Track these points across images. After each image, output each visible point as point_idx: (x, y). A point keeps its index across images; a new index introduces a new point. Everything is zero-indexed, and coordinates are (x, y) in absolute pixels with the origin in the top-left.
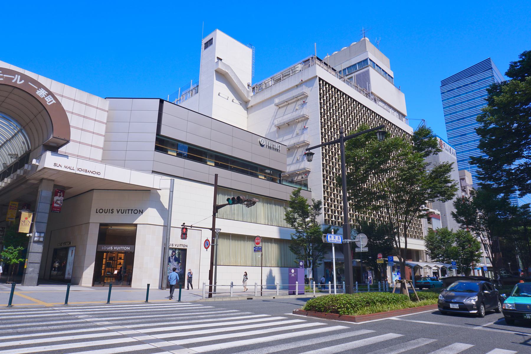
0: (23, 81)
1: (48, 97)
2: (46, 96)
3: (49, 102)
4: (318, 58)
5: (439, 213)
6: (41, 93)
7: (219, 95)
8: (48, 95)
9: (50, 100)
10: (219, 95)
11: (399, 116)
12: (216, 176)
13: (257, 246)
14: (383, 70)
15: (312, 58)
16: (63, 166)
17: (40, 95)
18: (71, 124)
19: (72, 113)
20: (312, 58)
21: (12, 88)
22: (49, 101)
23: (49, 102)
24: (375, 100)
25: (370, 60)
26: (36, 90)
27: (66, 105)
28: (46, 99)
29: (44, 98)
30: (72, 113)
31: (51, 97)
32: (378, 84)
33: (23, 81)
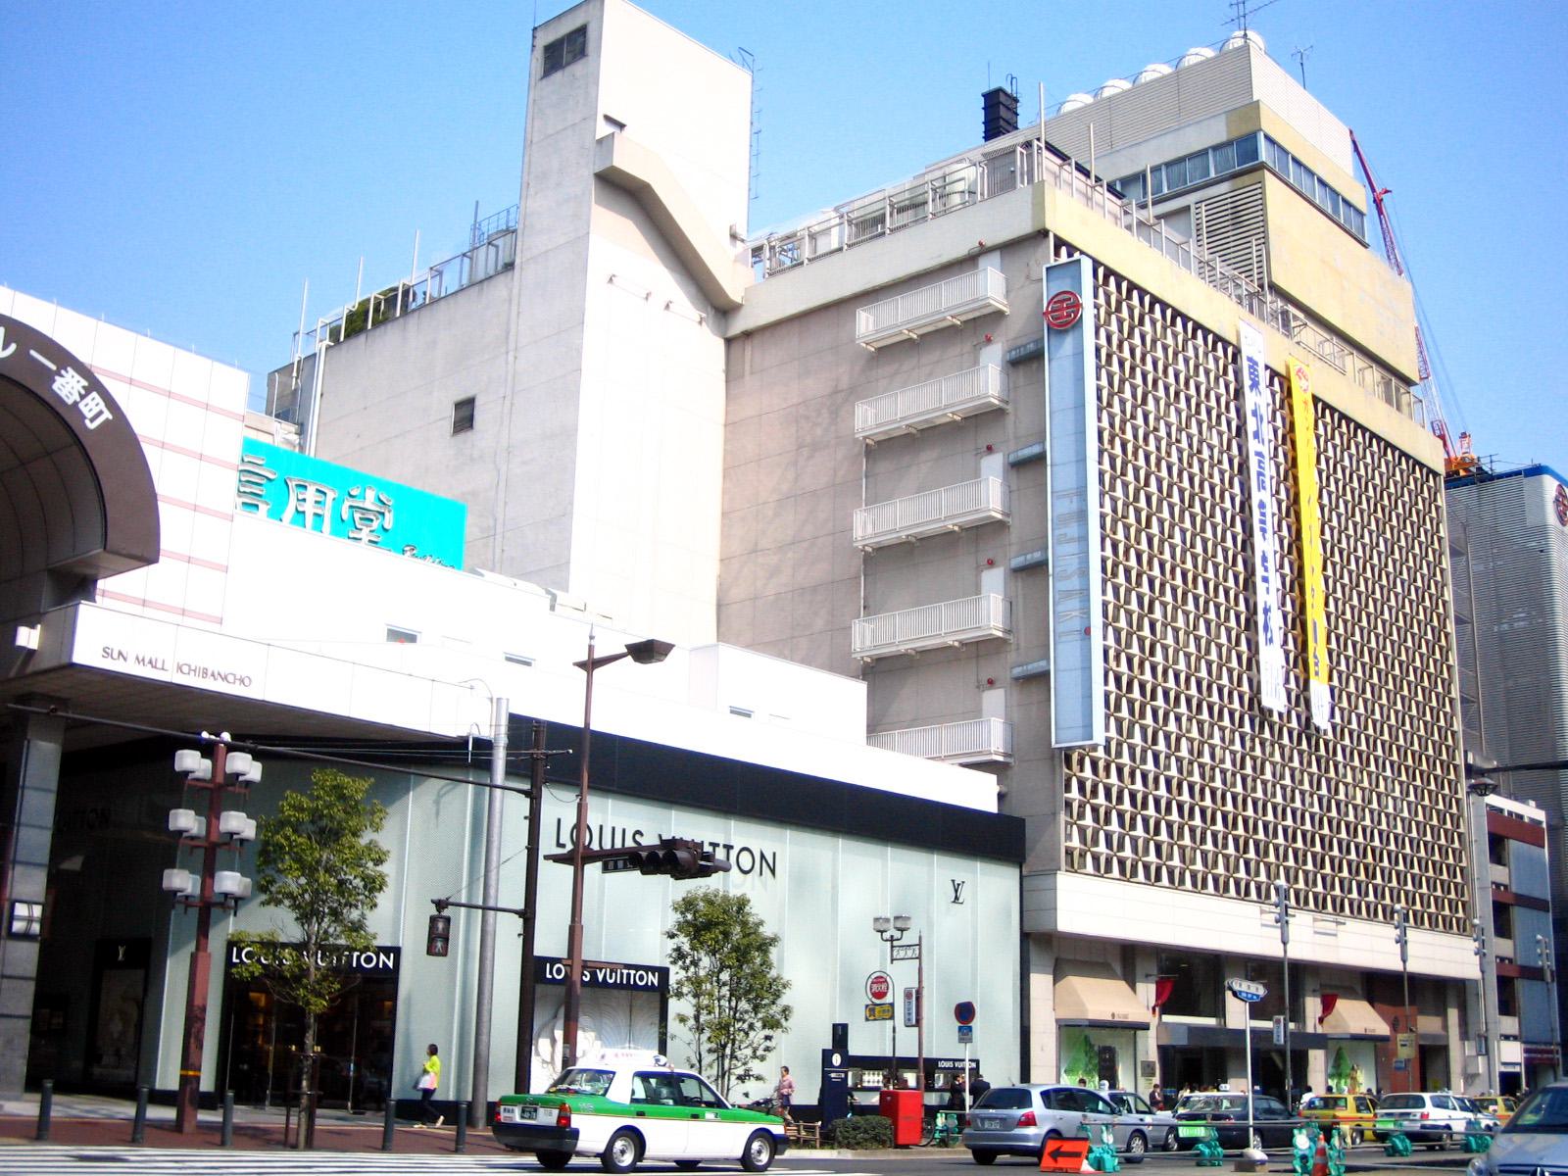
0: (13, 347)
1: (88, 399)
2: (82, 397)
3: (92, 420)
4: (1050, 148)
5: (1540, 815)
6: (68, 386)
7: (667, 307)
8: (88, 390)
9: (96, 410)
10: (667, 307)
11: (1388, 384)
12: (663, 1050)
13: (878, 1002)
14: (1321, 182)
15: (1028, 145)
16: (131, 659)
17: (63, 394)
18: (159, 489)
19: (163, 445)
20: (1028, 145)
21: (69, 440)
22: (92, 409)
23: (92, 420)
24: (1286, 324)
25: (1267, 137)
26: (49, 377)
27: (143, 419)
28: (81, 405)
29: (76, 404)
30: (163, 445)
31: (98, 399)
32: (1299, 242)
33: (13, 347)
